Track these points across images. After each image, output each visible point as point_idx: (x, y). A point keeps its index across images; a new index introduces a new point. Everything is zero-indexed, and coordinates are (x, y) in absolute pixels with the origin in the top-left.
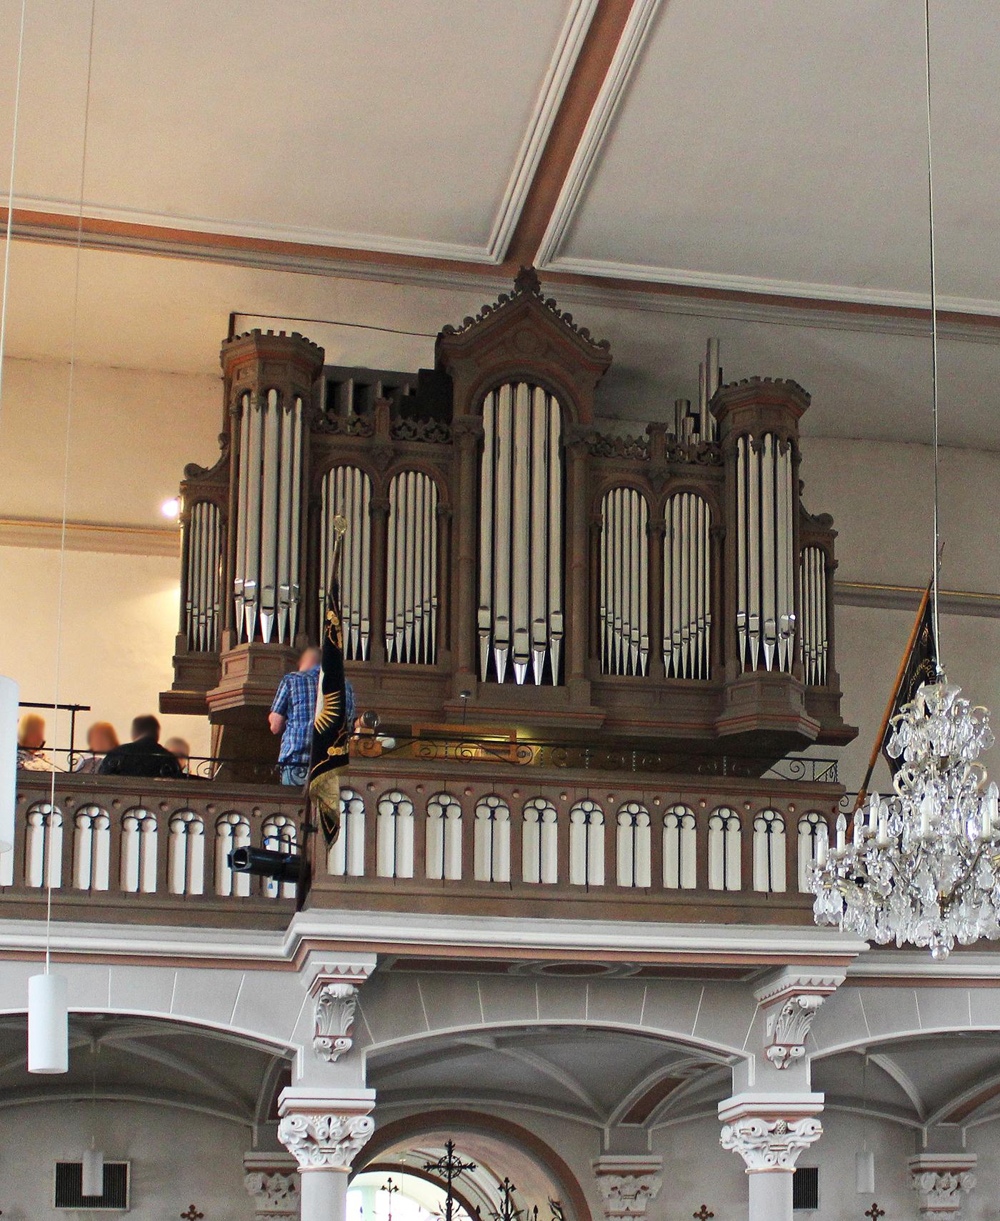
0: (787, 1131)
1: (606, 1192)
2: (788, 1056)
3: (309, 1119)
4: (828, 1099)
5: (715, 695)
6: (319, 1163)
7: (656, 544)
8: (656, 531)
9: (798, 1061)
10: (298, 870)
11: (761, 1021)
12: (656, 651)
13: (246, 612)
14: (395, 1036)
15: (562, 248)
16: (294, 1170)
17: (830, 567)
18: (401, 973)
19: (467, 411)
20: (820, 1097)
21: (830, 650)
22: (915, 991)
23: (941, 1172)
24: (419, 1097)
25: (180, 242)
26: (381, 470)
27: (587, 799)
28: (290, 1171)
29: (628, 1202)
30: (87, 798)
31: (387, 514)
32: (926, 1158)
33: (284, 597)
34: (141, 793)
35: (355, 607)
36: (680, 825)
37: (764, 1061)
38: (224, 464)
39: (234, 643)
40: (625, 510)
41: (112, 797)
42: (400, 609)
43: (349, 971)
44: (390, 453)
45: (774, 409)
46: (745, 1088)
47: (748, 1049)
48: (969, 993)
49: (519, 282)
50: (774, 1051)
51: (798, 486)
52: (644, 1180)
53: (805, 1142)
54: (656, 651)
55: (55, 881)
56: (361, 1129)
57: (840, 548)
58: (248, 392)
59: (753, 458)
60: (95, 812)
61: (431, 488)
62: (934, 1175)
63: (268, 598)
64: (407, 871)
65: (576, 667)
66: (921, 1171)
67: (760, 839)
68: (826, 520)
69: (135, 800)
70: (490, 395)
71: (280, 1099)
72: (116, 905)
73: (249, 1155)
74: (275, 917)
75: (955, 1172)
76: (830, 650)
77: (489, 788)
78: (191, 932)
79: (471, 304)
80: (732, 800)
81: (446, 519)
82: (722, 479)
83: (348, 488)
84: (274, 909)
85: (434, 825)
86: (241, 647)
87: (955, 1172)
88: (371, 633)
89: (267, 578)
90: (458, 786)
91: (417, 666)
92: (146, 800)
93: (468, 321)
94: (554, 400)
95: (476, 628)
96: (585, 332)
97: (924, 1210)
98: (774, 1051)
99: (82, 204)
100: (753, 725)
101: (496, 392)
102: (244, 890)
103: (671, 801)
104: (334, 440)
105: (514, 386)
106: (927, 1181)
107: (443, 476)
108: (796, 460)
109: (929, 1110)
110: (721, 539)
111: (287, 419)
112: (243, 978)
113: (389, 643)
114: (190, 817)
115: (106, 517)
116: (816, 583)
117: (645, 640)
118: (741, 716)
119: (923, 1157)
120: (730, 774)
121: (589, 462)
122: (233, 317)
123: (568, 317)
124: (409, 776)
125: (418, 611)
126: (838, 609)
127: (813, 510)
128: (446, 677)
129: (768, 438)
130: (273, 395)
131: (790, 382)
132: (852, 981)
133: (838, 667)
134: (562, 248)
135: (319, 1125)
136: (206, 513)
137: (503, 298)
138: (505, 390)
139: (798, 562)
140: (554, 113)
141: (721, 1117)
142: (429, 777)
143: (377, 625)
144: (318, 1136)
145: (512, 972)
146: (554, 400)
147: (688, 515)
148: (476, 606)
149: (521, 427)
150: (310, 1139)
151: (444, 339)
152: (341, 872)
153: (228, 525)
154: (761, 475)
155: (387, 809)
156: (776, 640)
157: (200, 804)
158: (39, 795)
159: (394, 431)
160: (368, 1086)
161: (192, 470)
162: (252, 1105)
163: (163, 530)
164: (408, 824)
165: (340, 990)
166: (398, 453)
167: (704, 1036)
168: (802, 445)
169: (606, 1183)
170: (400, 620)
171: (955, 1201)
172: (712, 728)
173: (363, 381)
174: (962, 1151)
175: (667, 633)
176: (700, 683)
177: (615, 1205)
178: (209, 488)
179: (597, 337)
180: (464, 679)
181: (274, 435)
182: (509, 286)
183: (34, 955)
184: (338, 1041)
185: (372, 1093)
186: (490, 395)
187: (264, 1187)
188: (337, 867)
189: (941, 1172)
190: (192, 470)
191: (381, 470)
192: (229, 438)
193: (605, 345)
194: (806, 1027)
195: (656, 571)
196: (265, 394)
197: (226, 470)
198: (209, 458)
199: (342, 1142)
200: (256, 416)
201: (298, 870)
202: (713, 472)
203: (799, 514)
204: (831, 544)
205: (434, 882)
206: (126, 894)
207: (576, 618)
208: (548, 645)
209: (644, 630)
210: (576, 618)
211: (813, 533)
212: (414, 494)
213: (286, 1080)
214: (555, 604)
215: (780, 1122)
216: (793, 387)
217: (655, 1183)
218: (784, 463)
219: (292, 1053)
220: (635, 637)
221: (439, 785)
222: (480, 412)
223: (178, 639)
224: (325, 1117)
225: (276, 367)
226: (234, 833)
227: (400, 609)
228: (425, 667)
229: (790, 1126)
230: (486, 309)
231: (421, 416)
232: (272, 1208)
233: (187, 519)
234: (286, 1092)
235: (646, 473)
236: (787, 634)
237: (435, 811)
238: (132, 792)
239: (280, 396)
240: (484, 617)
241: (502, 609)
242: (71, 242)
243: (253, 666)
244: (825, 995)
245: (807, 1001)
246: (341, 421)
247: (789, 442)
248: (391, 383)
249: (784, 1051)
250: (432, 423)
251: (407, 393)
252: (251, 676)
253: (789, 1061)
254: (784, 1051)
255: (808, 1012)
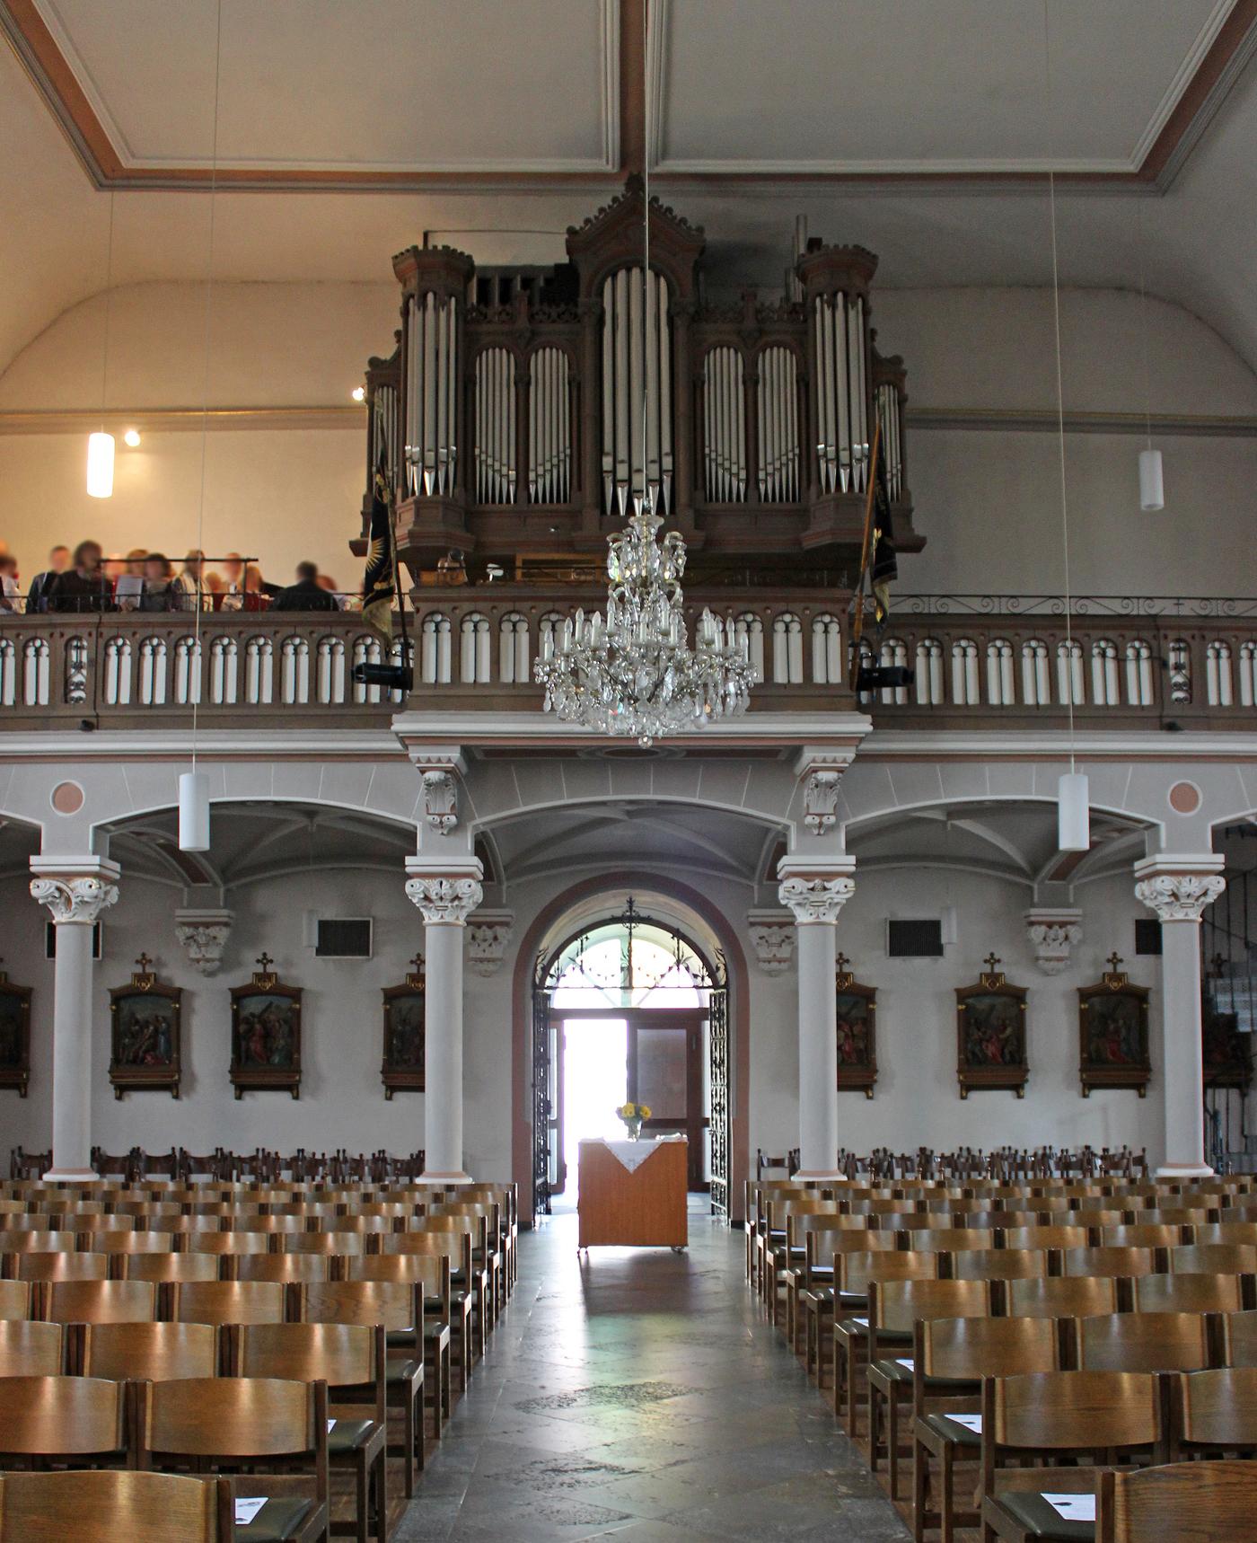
0: (825, 889)
1: (755, 940)
2: (821, 825)
3: (426, 882)
4: (859, 863)
5: (803, 516)
6: (436, 919)
7: (750, 393)
8: (751, 381)
9: (832, 828)
10: (402, 678)
11: (799, 797)
12: (752, 480)
13: (413, 471)
14: (494, 812)
15: (664, 153)
16: (792, 924)
17: (902, 401)
18: (484, 764)
19: (589, 295)
20: (852, 859)
21: (903, 471)
22: (938, 767)
23: (1050, 925)
24: (567, 865)
25: (369, 181)
26: (523, 350)
27: (514, 611)
28: (789, 923)
29: (774, 949)
30: (256, 631)
31: (529, 384)
32: (1037, 913)
33: (443, 458)
34: (295, 624)
35: (734, 459)
36: (787, 631)
37: (804, 829)
38: (398, 354)
39: (405, 497)
40: (724, 365)
41: (273, 629)
42: (540, 460)
43: (834, 761)
44: (528, 335)
45: (847, 271)
46: (1158, 850)
47: (790, 817)
48: (987, 768)
49: (628, 185)
50: (809, 819)
51: (870, 335)
52: (213, 931)
53: (841, 899)
54: (752, 480)
55: (196, 698)
56: (466, 890)
57: (909, 387)
58: (821, 295)
59: (828, 313)
60: (297, 641)
61: (564, 361)
62: (1043, 928)
63: (430, 456)
64: (485, 677)
65: (683, 498)
66: (1032, 924)
67: (779, 638)
68: (897, 360)
69: (290, 631)
70: (609, 281)
71: (780, 865)
72: (243, 715)
73: (179, 912)
74: (379, 718)
75: (1062, 925)
76: (903, 471)
77: (550, 606)
78: (338, 733)
79: (586, 208)
80: (754, 606)
81: (575, 384)
82: (806, 333)
83: (497, 366)
84: (147, 712)
85: (507, 638)
86: (410, 500)
87: (1062, 925)
88: (517, 482)
89: (429, 443)
90: (526, 606)
91: (555, 506)
92: (299, 630)
93: (587, 221)
94: (662, 280)
95: (600, 472)
96: (683, 221)
97: (1037, 959)
98: (809, 819)
99: (214, 159)
100: (827, 540)
101: (614, 276)
102: (375, 698)
103: (504, 610)
104: (485, 327)
105: (629, 270)
106: (1037, 933)
107: (572, 350)
108: (866, 313)
109: (1036, 869)
110: (805, 385)
111: (443, 315)
112: (374, 768)
113: (762, 487)
114: (334, 641)
115: (313, 403)
116: (891, 414)
117: (513, 473)
118: (819, 533)
119: (1033, 911)
120: (752, 584)
121: (692, 327)
122: (426, 235)
123: (669, 210)
124: (485, 599)
125: (555, 461)
126: (909, 433)
127: (885, 349)
128: (575, 516)
129: (840, 296)
130: (840, 296)
131: (856, 247)
132: (861, 758)
133: (911, 485)
134: (597, 153)
135: (433, 887)
136: (385, 396)
137: (615, 200)
138: (622, 275)
139: (871, 399)
140: (617, 44)
141: (1137, 875)
142: (502, 599)
143: (522, 474)
144: (434, 897)
145: (782, 757)
146: (662, 280)
147: (778, 365)
148: (601, 452)
149: (637, 304)
150: (426, 898)
151: (575, 240)
152: (432, 680)
153: (401, 402)
154: (836, 328)
155: (468, 627)
156: (850, 466)
157: (339, 630)
158: (184, 631)
159: (531, 317)
160: (1215, 850)
161: (374, 362)
162: (753, 868)
163: (354, 407)
164: (485, 639)
165: (433, 776)
166: (534, 334)
167: (752, 807)
168: (874, 300)
169: (755, 933)
170: (770, 469)
171: (1064, 951)
172: (798, 542)
173: (506, 276)
174: (1069, 906)
175: (761, 465)
176: (790, 506)
177: (764, 953)
178: (385, 375)
179: (692, 223)
180: (591, 515)
181: (438, 327)
182: (619, 189)
183: (184, 757)
184: (825, 819)
185: (852, 859)
186: (609, 281)
187: (473, 937)
188: (430, 677)
189: (1050, 925)
190: (374, 362)
191: (523, 350)
192: (402, 336)
193: (700, 230)
194: (833, 799)
195: (751, 415)
196: (424, 297)
197: (401, 357)
198: (387, 353)
199: (453, 900)
200: (419, 315)
201: (402, 678)
202: (797, 329)
203: (872, 358)
204: (902, 381)
205: (506, 685)
206: (323, 706)
207: (682, 457)
208: (661, 482)
209: (742, 463)
210: (682, 457)
211: (883, 372)
212: (549, 365)
213: (782, 850)
214: (666, 447)
215: (817, 881)
216: (859, 250)
217: (1073, 931)
218: (855, 317)
219: (787, 827)
220: (734, 469)
221: (509, 606)
222: (601, 294)
223: (365, 497)
224: (436, 882)
225: (434, 272)
226: (368, 652)
227: (540, 460)
228: (562, 506)
229: (827, 885)
230: (602, 210)
231: (554, 302)
232: (481, 955)
233: (370, 402)
234: (785, 860)
235: (739, 333)
236: (860, 460)
237: (507, 627)
238: (288, 624)
239: (845, 296)
240: (607, 463)
241: (622, 455)
242: (207, 189)
243: (417, 515)
244: (840, 771)
245: (825, 776)
246: (490, 312)
247: (857, 296)
248: (528, 276)
249: (817, 820)
250: (563, 307)
251: (542, 283)
252: (415, 523)
253: (826, 829)
254: (817, 820)
255: (830, 785)
